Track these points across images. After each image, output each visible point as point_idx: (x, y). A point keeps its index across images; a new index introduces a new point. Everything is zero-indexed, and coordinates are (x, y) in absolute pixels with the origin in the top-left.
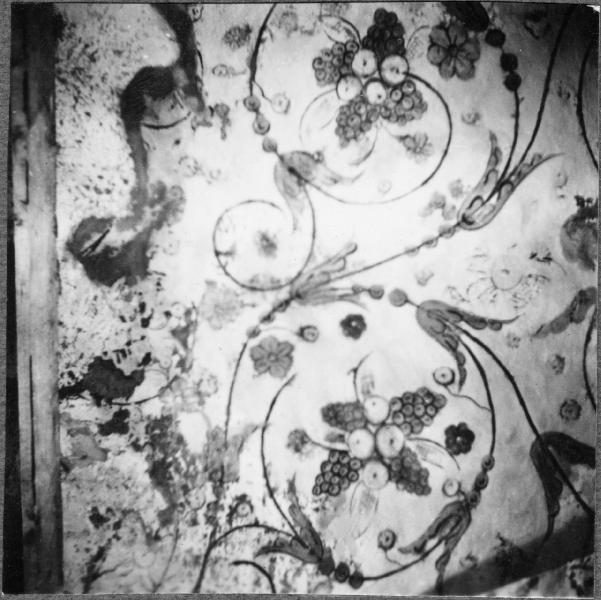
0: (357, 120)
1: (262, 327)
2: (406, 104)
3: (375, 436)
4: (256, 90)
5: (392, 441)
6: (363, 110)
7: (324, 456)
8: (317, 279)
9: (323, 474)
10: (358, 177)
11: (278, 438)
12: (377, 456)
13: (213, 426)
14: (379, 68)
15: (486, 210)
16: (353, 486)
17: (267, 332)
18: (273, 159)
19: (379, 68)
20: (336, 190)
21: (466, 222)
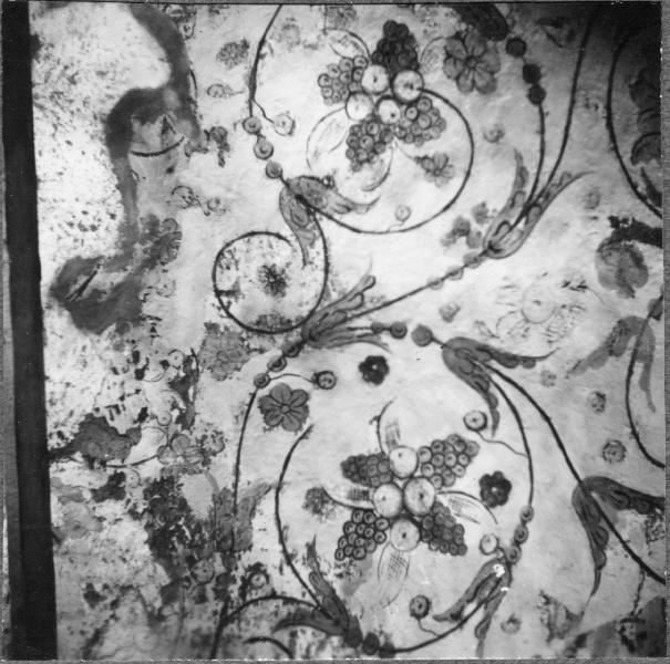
1: (272, 375)
2: (423, 123)
3: (403, 491)
4: (256, 110)
5: (422, 496)
7: (347, 515)
8: (331, 319)
9: (346, 536)
10: (373, 203)
12: (405, 513)
15: (514, 236)
20: (349, 219)
21: (493, 250)
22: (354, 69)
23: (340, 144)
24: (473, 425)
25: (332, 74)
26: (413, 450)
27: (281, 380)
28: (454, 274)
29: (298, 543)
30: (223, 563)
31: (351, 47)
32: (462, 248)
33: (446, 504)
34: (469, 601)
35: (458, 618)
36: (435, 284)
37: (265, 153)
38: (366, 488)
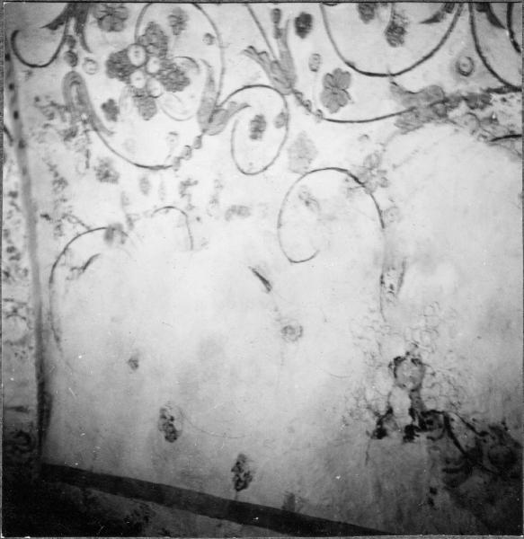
0: (172, 76)
1: (314, 109)
2: (154, 40)
4: (168, 163)
6: (165, 73)
10: (205, 62)
11: (398, 58)
14: (138, 67)
17: (318, 105)
18: (206, 139)
19: (138, 67)
23: (176, 97)
30: (457, 107)
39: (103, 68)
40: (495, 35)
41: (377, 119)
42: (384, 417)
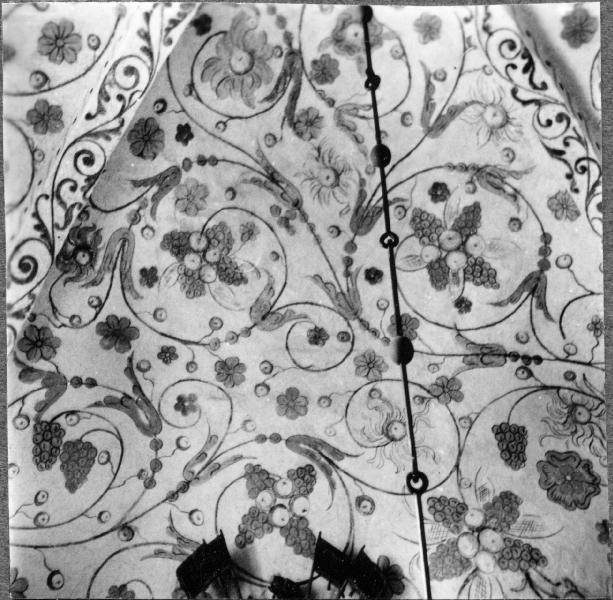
1: (382, 336)
3: (449, 252)
4: (205, 341)
5: (450, 239)
7: (469, 285)
8: (342, 302)
9: (483, 283)
10: (268, 273)
12: (462, 248)
13: (463, 365)
14: (197, 252)
15: (290, 190)
16: (486, 260)
20: (278, 288)
21: (297, 204)
22: (185, 274)
24: (403, 213)
25: (187, 288)
26: (422, 250)
27: (385, 331)
28: (312, 228)
29: (494, 314)
31: (172, 275)
32: (296, 223)
33: (452, 223)
34: (504, 191)
35: (515, 196)
36: (318, 240)
37: (234, 338)
38: (451, 275)
39: (159, 239)
40: (547, 325)
41: (437, 324)
42: (265, 64)
